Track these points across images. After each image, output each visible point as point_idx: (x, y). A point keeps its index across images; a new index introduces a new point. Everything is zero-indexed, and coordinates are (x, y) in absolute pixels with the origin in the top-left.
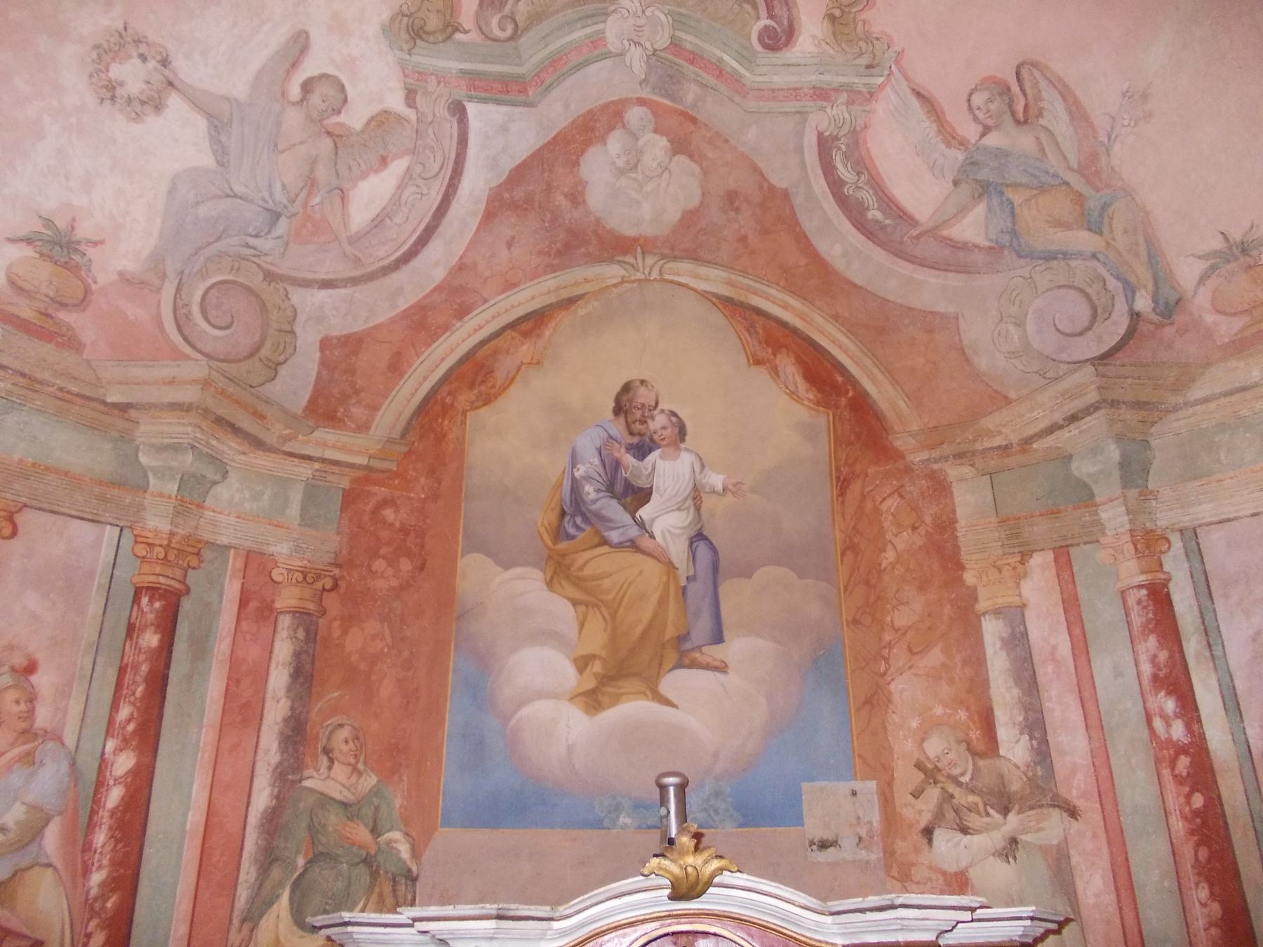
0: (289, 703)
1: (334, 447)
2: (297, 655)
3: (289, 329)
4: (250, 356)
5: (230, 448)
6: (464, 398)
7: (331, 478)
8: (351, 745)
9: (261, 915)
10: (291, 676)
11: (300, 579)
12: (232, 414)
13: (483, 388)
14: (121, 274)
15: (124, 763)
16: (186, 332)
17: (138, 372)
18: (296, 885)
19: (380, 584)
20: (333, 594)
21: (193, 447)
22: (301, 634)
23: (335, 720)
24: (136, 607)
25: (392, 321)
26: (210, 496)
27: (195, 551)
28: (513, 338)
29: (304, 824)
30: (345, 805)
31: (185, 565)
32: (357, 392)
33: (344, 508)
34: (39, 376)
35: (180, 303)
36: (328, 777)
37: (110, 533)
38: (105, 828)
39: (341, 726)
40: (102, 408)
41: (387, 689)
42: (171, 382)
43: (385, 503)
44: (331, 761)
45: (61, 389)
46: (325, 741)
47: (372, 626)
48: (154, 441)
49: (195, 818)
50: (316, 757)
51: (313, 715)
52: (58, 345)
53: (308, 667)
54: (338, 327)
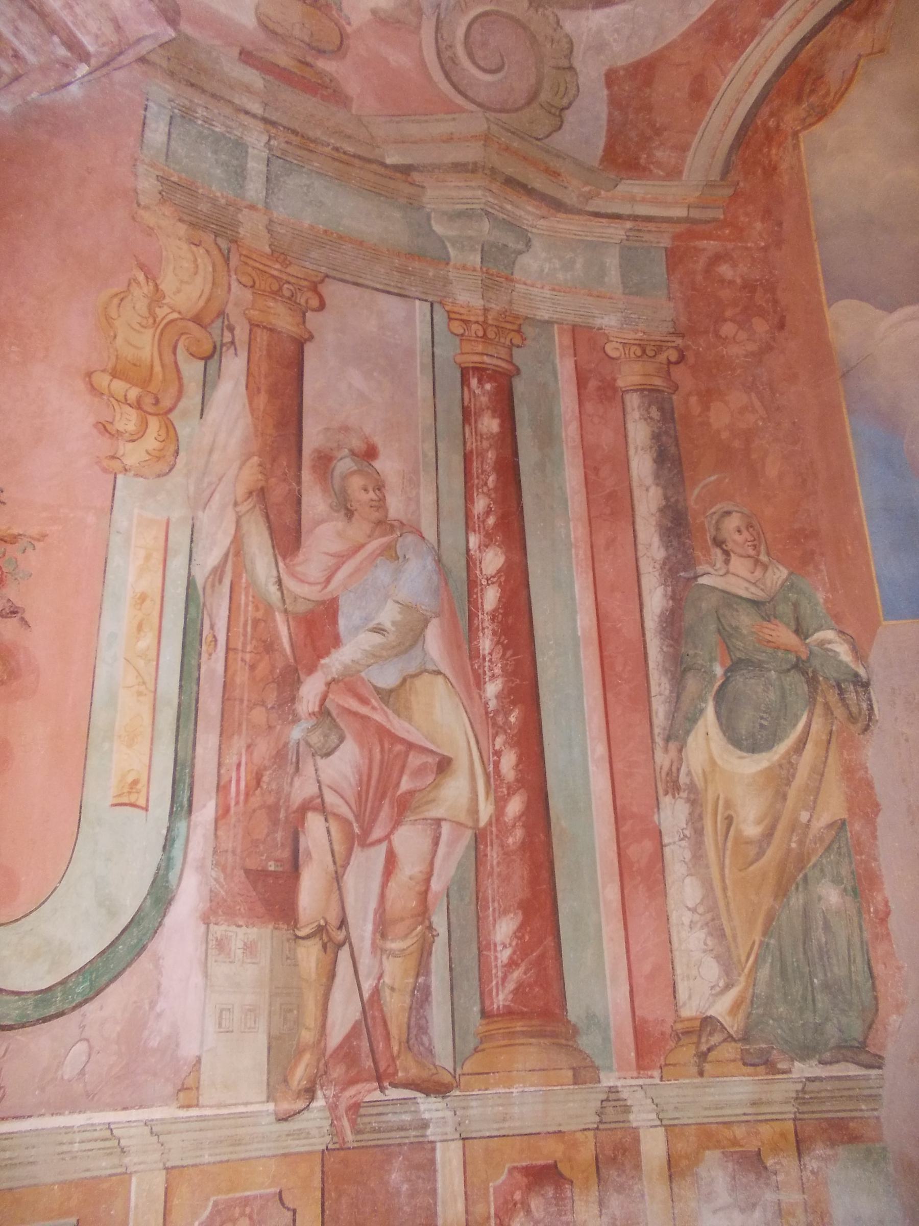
0: (660, 491)
1: (643, 200)
2: (656, 437)
3: (566, 64)
4: (529, 103)
5: (529, 213)
6: (790, 118)
7: (647, 237)
8: (746, 534)
9: (688, 733)
10: (655, 461)
11: (639, 353)
12: (520, 170)
13: (813, 99)
14: (374, 12)
15: (492, 561)
16: (455, 79)
17: (412, 129)
18: (720, 697)
19: (734, 350)
20: (682, 365)
21: (487, 213)
22: (655, 413)
23: (719, 507)
24: (466, 389)
25: (686, 36)
26: (517, 267)
27: (515, 327)
28: (843, 27)
29: (713, 627)
30: (756, 603)
31: (508, 342)
32: (658, 132)
33: (671, 268)
34: (311, 134)
35: (443, 45)
36: (727, 572)
37: (421, 309)
38: (488, 632)
39: (728, 513)
40: (382, 170)
41: (772, 470)
42: (449, 139)
43: (717, 258)
44: (727, 553)
45: (337, 149)
46: (713, 532)
47: (737, 398)
48: (445, 207)
49: (585, 621)
50: (708, 552)
51: (692, 502)
52: (323, 98)
53: (673, 450)
54: (623, 54)
